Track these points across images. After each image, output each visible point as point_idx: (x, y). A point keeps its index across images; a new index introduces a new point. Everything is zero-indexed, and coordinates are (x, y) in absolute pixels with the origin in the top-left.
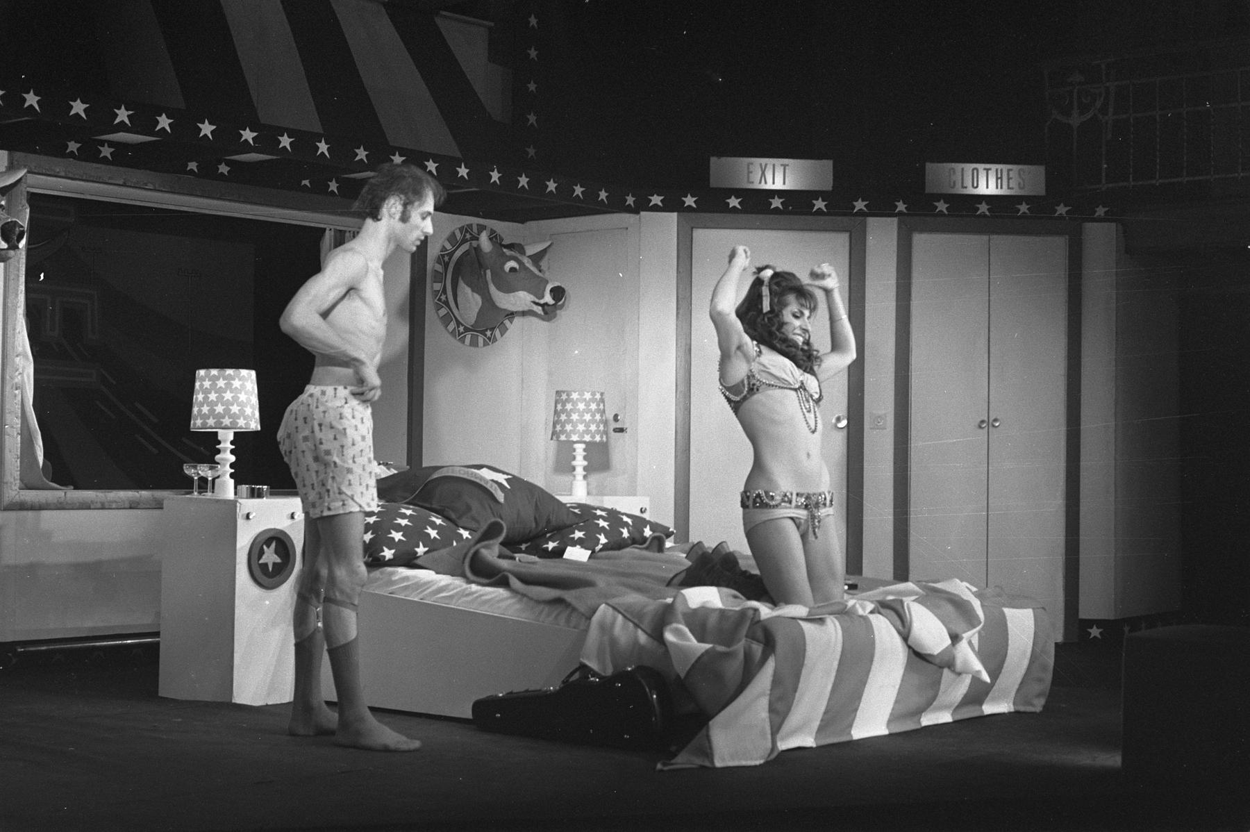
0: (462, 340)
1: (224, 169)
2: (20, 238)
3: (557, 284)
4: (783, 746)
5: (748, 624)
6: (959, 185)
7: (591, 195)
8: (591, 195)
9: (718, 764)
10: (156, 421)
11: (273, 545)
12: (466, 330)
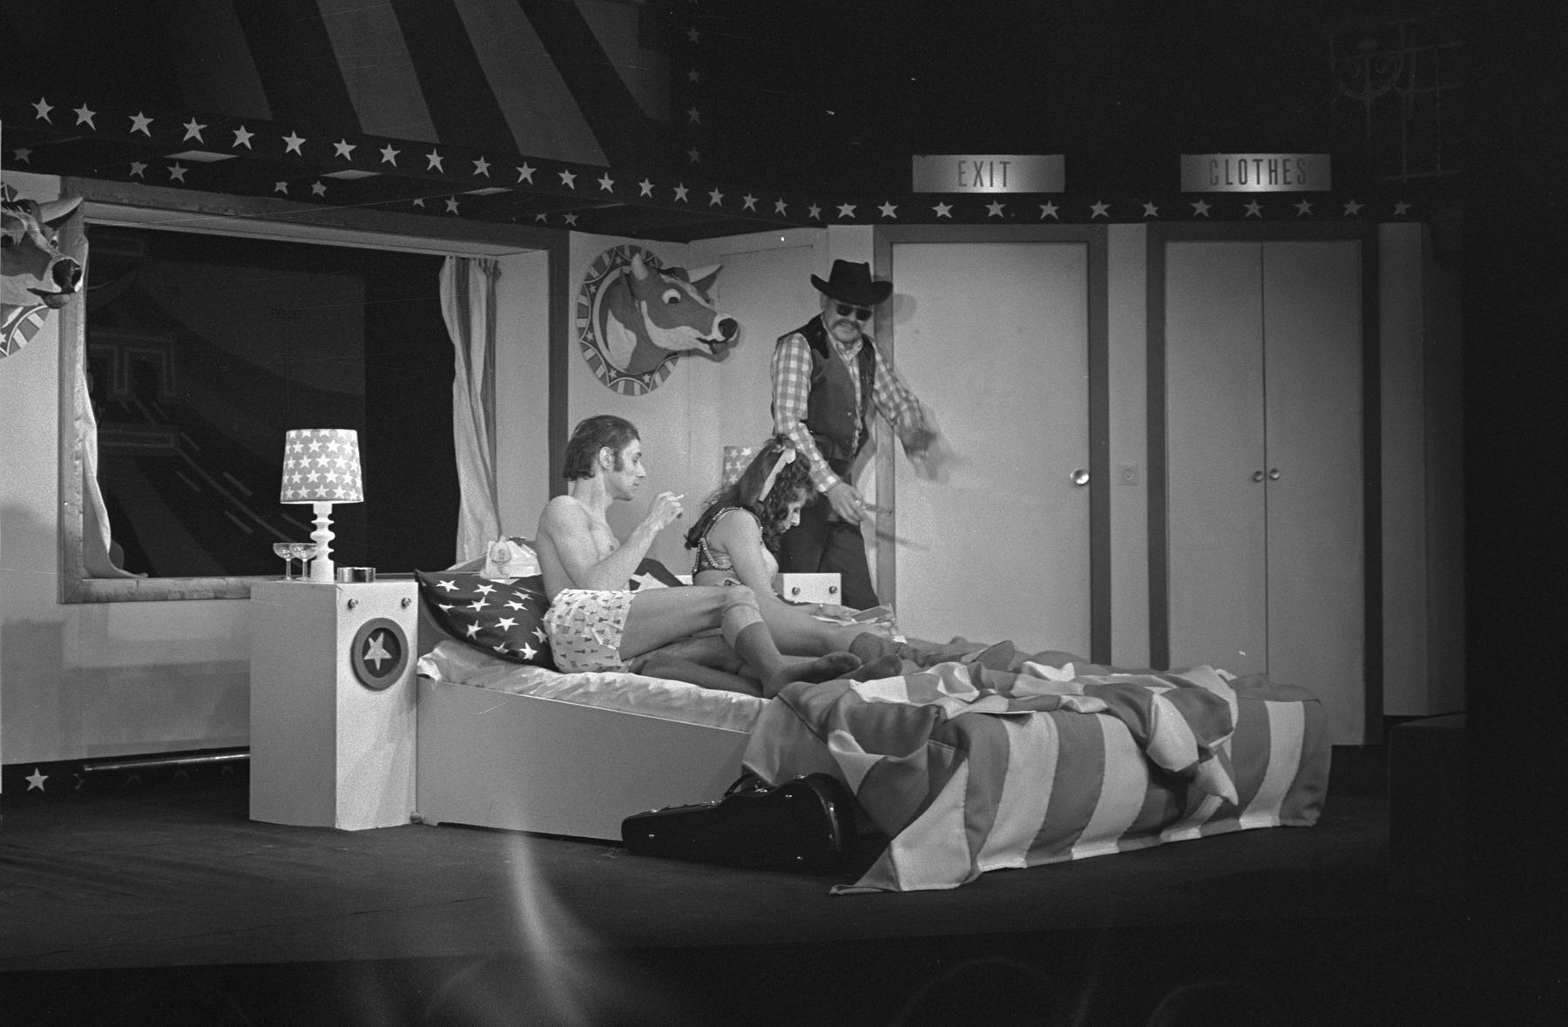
0: (614, 388)
1: (319, 189)
2: (76, 279)
3: (727, 316)
4: (985, 866)
5: (931, 726)
6: (1222, 180)
7: (765, 206)
8: (765, 206)
9: (905, 888)
10: (249, 493)
11: (381, 638)
12: (619, 374)
